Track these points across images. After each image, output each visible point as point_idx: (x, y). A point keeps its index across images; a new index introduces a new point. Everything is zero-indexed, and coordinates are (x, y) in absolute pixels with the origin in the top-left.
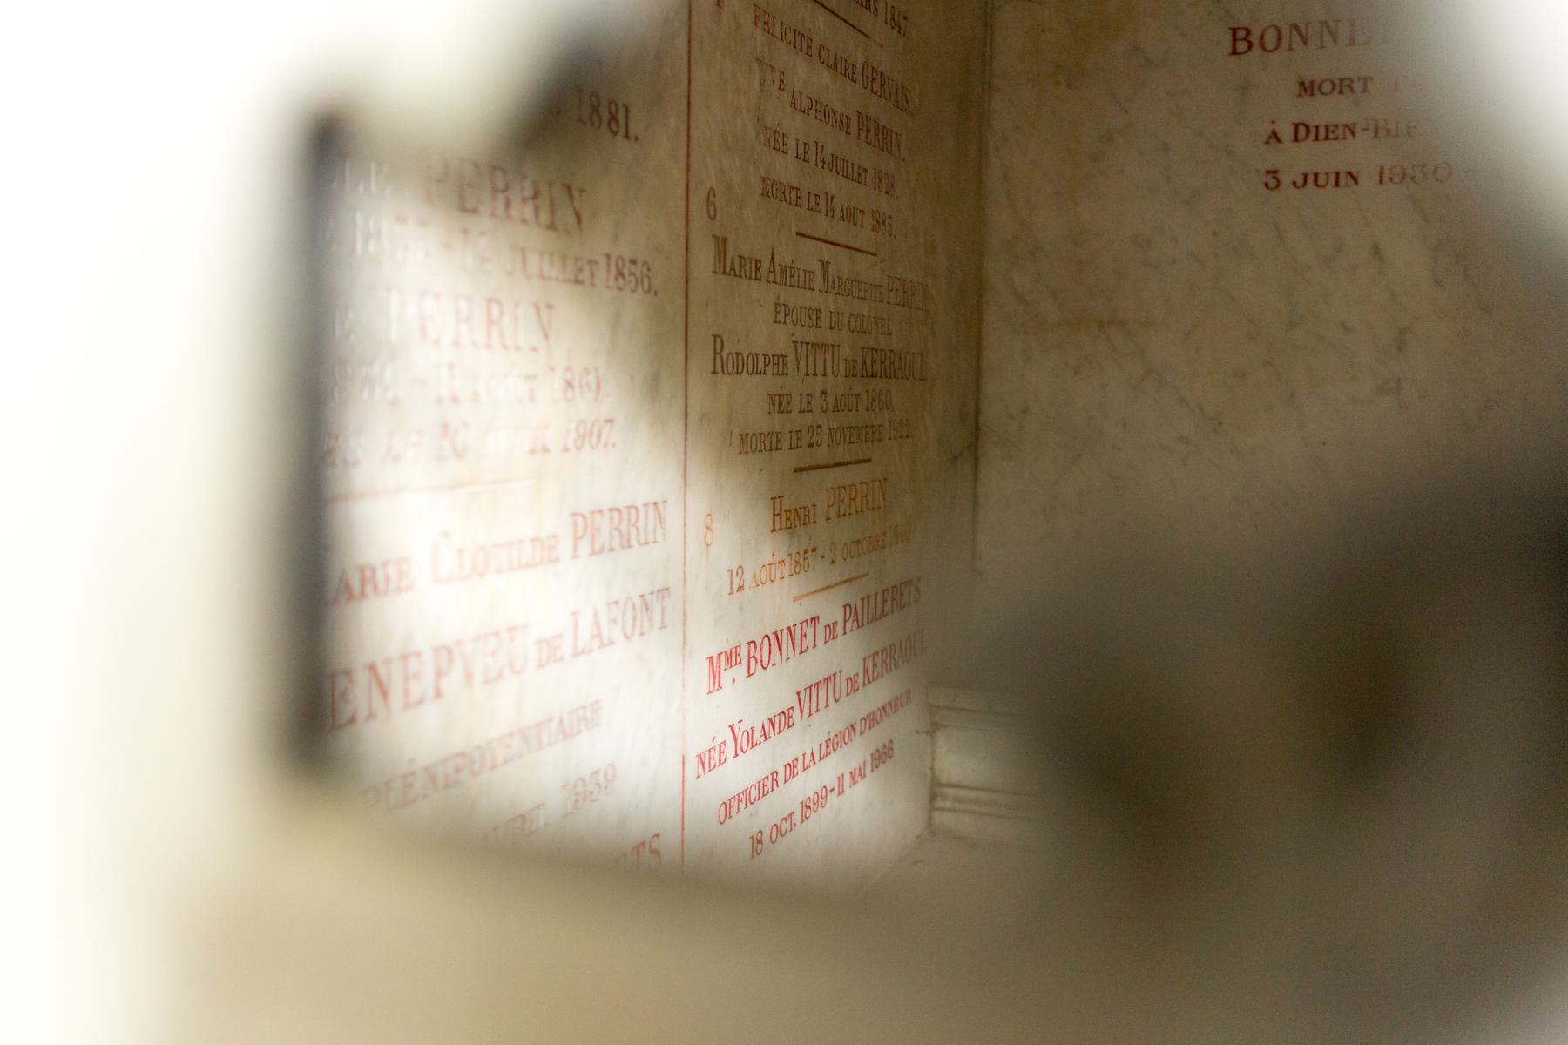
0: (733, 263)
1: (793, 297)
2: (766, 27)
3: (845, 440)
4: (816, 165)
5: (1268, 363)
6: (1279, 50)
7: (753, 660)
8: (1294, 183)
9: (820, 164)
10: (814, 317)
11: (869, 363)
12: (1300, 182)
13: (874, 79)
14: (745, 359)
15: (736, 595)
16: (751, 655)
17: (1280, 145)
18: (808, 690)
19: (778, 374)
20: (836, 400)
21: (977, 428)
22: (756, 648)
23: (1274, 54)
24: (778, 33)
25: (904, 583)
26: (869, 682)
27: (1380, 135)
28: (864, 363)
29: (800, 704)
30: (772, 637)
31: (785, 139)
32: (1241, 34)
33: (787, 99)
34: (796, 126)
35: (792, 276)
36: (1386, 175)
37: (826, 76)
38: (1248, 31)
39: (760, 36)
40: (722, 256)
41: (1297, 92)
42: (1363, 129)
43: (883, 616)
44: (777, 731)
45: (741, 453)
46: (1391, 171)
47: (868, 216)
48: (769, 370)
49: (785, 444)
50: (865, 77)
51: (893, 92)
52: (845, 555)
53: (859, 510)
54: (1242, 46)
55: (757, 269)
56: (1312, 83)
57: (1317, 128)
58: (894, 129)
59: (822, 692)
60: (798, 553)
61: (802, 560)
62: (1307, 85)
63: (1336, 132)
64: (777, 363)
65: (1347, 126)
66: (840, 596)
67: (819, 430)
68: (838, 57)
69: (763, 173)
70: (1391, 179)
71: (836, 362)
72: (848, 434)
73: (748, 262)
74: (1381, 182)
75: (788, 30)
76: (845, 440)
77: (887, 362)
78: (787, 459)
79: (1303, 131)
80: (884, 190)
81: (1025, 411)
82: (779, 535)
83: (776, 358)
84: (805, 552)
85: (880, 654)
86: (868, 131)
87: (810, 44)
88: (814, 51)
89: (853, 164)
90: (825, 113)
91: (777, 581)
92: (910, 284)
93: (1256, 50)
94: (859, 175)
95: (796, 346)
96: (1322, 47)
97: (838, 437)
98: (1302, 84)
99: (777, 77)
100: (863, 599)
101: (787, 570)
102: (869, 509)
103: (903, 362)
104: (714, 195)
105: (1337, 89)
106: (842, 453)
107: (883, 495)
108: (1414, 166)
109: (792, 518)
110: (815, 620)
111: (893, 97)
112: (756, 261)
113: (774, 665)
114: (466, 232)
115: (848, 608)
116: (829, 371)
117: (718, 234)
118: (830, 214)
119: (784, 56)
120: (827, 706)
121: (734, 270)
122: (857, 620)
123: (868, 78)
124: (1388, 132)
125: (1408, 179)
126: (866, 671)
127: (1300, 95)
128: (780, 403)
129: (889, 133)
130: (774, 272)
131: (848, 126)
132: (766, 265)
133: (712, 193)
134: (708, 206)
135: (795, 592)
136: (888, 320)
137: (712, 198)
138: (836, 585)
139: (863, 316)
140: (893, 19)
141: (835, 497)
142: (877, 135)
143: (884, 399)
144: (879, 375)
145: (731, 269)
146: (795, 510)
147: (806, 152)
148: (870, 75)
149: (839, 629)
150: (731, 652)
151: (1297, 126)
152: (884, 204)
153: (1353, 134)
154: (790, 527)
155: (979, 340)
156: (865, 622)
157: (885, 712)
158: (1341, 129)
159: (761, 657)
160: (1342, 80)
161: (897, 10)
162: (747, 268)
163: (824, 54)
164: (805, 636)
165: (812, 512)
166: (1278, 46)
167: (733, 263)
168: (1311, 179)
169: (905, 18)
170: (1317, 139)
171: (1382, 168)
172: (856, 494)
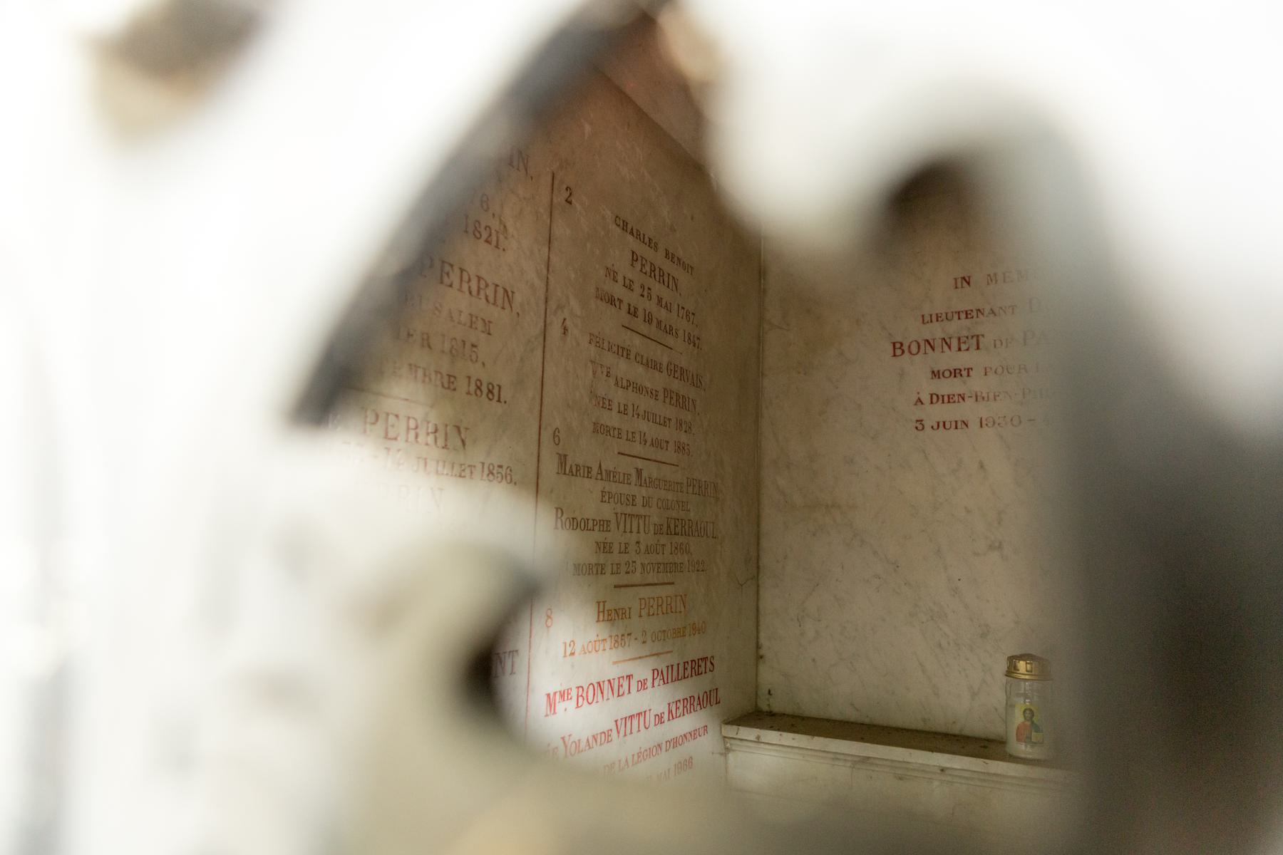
0: (645, 480)
1: (614, 488)
4: (633, 416)
7: (580, 699)
8: (932, 427)
9: (636, 416)
11: (672, 526)
13: (676, 371)
15: (569, 658)
16: (580, 694)
18: (624, 720)
19: (603, 531)
21: (758, 567)
22: (583, 690)
23: (915, 356)
24: (606, 348)
25: (701, 659)
26: (673, 718)
28: (669, 527)
29: (617, 728)
30: (596, 685)
32: (898, 345)
33: (612, 381)
36: (984, 423)
37: (640, 369)
38: (902, 344)
39: (593, 348)
40: (563, 465)
43: (684, 678)
44: (599, 743)
45: (574, 575)
47: (671, 445)
48: (597, 528)
49: (608, 570)
50: (669, 371)
51: (690, 377)
52: (654, 639)
53: (665, 612)
54: (898, 352)
59: (635, 722)
60: (618, 636)
61: (620, 640)
64: (604, 525)
66: (652, 663)
67: (634, 564)
68: (649, 359)
69: (594, 420)
70: (987, 425)
72: (656, 567)
73: (582, 468)
74: (981, 426)
78: (609, 579)
79: (935, 398)
80: (684, 430)
82: (602, 624)
84: (623, 635)
85: (682, 702)
86: (671, 398)
88: (632, 356)
89: (660, 417)
90: (639, 389)
91: (601, 651)
94: (665, 422)
96: (942, 352)
98: (933, 372)
99: (605, 371)
100: (668, 667)
101: (607, 645)
102: (672, 612)
104: (559, 431)
105: (953, 375)
106: (651, 578)
108: (999, 418)
109: (613, 614)
110: (629, 677)
111: (690, 381)
112: (588, 468)
113: (597, 702)
114: (388, 449)
115: (656, 671)
117: (560, 452)
119: (609, 359)
120: (639, 731)
121: (572, 472)
122: (663, 679)
125: (996, 425)
126: (670, 712)
127: (932, 378)
128: (604, 547)
129: (687, 399)
130: (601, 473)
132: (595, 470)
134: (554, 438)
135: (615, 659)
137: (557, 433)
138: (647, 656)
139: (668, 500)
142: (680, 401)
144: (680, 534)
146: (615, 610)
148: (672, 368)
149: (649, 683)
150: (564, 692)
151: (932, 395)
152: (684, 438)
153: (963, 399)
155: (758, 517)
156: (670, 680)
157: (686, 738)
158: (956, 397)
159: (587, 696)
160: (955, 370)
161: (692, 335)
162: (582, 471)
164: (622, 686)
165: (628, 612)
166: (918, 352)
167: (645, 480)
168: (941, 425)
169: (698, 338)
170: (943, 402)
171: (981, 419)
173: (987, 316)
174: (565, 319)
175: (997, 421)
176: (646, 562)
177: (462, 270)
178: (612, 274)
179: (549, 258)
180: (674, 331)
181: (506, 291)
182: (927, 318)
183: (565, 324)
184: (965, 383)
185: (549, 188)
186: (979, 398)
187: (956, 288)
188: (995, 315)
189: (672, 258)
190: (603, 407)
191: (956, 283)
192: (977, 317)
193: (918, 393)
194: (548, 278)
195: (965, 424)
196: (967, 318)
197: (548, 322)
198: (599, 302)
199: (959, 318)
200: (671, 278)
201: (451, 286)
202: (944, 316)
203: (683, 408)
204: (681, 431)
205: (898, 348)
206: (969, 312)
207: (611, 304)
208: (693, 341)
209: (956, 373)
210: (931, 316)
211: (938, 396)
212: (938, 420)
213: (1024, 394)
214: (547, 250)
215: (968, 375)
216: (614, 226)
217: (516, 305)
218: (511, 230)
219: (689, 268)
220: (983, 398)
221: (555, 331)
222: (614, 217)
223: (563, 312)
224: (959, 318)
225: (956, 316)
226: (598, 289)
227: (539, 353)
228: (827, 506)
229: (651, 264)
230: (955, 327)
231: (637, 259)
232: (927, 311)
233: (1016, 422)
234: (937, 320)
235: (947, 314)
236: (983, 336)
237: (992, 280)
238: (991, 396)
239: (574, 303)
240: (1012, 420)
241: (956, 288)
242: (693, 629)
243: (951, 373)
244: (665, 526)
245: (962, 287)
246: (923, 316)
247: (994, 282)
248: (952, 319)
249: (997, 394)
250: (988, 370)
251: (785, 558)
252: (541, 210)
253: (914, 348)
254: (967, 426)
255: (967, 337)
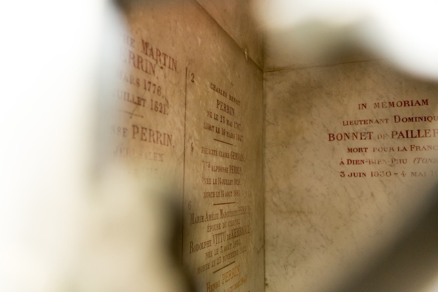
0: (224, 215)
2: (205, 152)
3: (227, 258)
4: (219, 184)
5: (345, 225)
6: (342, 140)
8: (349, 176)
9: (220, 183)
10: (218, 226)
12: (350, 175)
13: (235, 156)
14: (199, 249)
17: (344, 165)
20: (225, 248)
21: (264, 241)
23: (339, 141)
24: (208, 153)
27: (370, 163)
31: (210, 180)
32: (331, 135)
33: (211, 169)
34: (213, 176)
35: (212, 217)
36: (373, 174)
37: (221, 159)
38: (333, 135)
39: (203, 155)
41: (348, 151)
42: (366, 162)
46: (374, 173)
50: (232, 156)
54: (332, 139)
55: (203, 219)
56: (351, 149)
57: (354, 161)
58: (239, 167)
62: (350, 149)
63: (359, 162)
65: (361, 161)
68: (224, 153)
69: (204, 192)
71: (225, 237)
74: (372, 176)
75: (211, 151)
76: (227, 258)
77: (239, 232)
79: (350, 162)
80: (237, 184)
81: (278, 236)
83: (208, 242)
87: (217, 152)
88: (218, 154)
92: (245, 207)
93: (336, 139)
94: (230, 182)
95: (213, 237)
96: (353, 139)
97: (226, 258)
98: (349, 149)
99: (208, 164)
102: (234, 276)
103: (243, 230)
104: (191, 203)
105: (358, 151)
107: (238, 270)
108: (380, 172)
111: (239, 159)
116: (223, 241)
118: (223, 196)
121: (196, 221)
123: (232, 155)
124: (373, 163)
125: (379, 175)
127: (348, 152)
129: (238, 168)
130: (207, 218)
131: (227, 170)
133: (190, 202)
136: (239, 219)
137: (190, 203)
140: (239, 138)
141: (225, 276)
142: (235, 170)
143: (238, 242)
145: (195, 221)
147: (216, 182)
151: (348, 160)
153: (363, 163)
154: (212, 290)
158: (360, 161)
160: (359, 149)
163: (220, 154)
168: (353, 174)
170: (354, 164)
171: (372, 172)
172: (231, 273)
173: (375, 123)
174: (192, 143)
175: (380, 174)
176: (225, 256)
177: (150, 130)
178: (209, 114)
179: (185, 113)
180: (233, 136)
181: (168, 136)
182: (346, 123)
183: (192, 146)
184: (364, 155)
185: (185, 76)
186: (371, 162)
187: (360, 109)
188: (378, 123)
189: (232, 99)
190: (207, 184)
191: (359, 107)
192: (370, 123)
193: (342, 159)
194: (185, 124)
195: (364, 174)
196: (365, 124)
197: (186, 146)
198: (205, 130)
199: (361, 124)
200: (232, 109)
201: (146, 140)
202: (354, 122)
203: (237, 173)
204: (236, 185)
205: (332, 137)
206: (366, 121)
207: (210, 130)
208: (240, 139)
209: (360, 150)
210: (347, 122)
211: (351, 161)
212: (351, 172)
213: (392, 161)
214: (184, 109)
215: (366, 151)
216: (210, 89)
217: (173, 142)
218: (170, 103)
219: (238, 102)
220: (373, 163)
221: (189, 150)
222: (210, 84)
223: (191, 139)
224: (361, 124)
225: (359, 123)
226: (204, 123)
227: (182, 164)
228: (298, 212)
229: (225, 104)
230: (359, 128)
231: (219, 104)
232: (346, 119)
233: (388, 174)
234: (351, 124)
235: (355, 121)
236: (372, 133)
237: (376, 106)
238: (377, 161)
239: (196, 134)
240: (387, 173)
241: (360, 109)
242: (242, 281)
243: (357, 150)
244: (231, 234)
245: (362, 109)
246: (344, 122)
247: (378, 107)
248: (358, 124)
249: (379, 161)
250: (375, 149)
251: (277, 237)
252: (182, 89)
253: (339, 137)
254: (365, 175)
255: (365, 133)
